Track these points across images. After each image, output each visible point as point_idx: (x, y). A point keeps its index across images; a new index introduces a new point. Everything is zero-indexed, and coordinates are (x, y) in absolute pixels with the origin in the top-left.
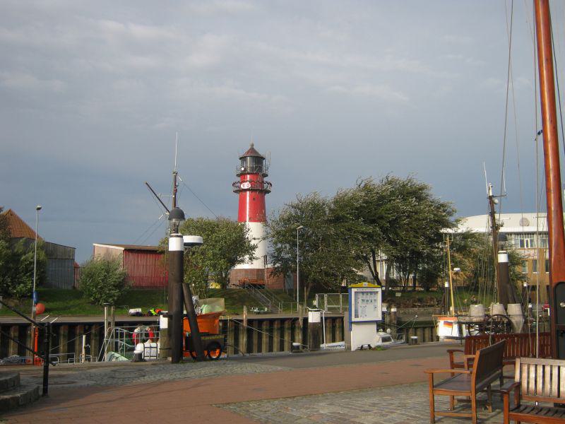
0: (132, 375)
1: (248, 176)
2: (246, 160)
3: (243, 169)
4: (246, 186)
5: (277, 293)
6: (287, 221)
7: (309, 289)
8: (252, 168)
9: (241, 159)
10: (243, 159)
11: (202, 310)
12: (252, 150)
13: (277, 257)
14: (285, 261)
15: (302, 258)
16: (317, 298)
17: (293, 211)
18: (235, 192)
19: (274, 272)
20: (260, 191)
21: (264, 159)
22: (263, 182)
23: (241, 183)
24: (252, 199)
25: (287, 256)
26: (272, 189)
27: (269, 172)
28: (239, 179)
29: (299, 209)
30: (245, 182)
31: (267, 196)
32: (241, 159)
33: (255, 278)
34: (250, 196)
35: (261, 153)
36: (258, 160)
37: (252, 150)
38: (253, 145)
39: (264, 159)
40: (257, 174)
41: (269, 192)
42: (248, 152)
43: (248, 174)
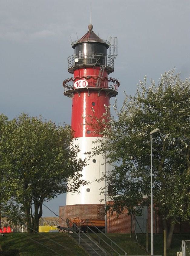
0: (80, 54)
1: (85, 71)
2: (81, 49)
3: (77, 60)
4: (82, 84)
5: (120, 239)
6: (138, 121)
7: (171, 235)
8: (90, 60)
9: (74, 47)
10: (78, 46)
11: (23, 215)
12: (91, 33)
13: (120, 182)
14: (132, 188)
15: (159, 184)
16: (184, 248)
17: (142, 107)
18: (67, 94)
19: (116, 206)
20: (103, 92)
21: (107, 46)
22: (106, 78)
23: (75, 81)
24: (91, 104)
25: (135, 180)
26: (119, 90)
27: (116, 66)
28: (72, 76)
29: (152, 104)
30: (79, 79)
31: (112, 100)
32: (74, 47)
33: (95, 217)
34: (88, 100)
35: (104, 37)
36: (100, 47)
37: (91, 33)
38: (91, 27)
39: (107, 46)
40: (97, 68)
41: (115, 94)
42: (85, 37)
43: (85, 67)
